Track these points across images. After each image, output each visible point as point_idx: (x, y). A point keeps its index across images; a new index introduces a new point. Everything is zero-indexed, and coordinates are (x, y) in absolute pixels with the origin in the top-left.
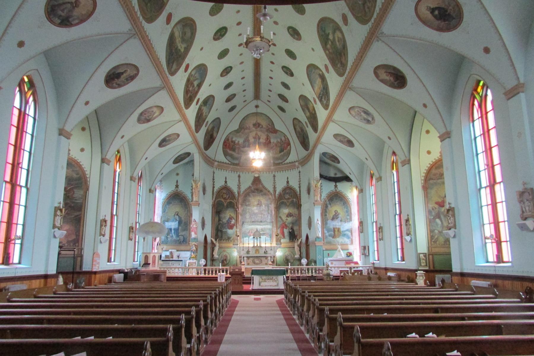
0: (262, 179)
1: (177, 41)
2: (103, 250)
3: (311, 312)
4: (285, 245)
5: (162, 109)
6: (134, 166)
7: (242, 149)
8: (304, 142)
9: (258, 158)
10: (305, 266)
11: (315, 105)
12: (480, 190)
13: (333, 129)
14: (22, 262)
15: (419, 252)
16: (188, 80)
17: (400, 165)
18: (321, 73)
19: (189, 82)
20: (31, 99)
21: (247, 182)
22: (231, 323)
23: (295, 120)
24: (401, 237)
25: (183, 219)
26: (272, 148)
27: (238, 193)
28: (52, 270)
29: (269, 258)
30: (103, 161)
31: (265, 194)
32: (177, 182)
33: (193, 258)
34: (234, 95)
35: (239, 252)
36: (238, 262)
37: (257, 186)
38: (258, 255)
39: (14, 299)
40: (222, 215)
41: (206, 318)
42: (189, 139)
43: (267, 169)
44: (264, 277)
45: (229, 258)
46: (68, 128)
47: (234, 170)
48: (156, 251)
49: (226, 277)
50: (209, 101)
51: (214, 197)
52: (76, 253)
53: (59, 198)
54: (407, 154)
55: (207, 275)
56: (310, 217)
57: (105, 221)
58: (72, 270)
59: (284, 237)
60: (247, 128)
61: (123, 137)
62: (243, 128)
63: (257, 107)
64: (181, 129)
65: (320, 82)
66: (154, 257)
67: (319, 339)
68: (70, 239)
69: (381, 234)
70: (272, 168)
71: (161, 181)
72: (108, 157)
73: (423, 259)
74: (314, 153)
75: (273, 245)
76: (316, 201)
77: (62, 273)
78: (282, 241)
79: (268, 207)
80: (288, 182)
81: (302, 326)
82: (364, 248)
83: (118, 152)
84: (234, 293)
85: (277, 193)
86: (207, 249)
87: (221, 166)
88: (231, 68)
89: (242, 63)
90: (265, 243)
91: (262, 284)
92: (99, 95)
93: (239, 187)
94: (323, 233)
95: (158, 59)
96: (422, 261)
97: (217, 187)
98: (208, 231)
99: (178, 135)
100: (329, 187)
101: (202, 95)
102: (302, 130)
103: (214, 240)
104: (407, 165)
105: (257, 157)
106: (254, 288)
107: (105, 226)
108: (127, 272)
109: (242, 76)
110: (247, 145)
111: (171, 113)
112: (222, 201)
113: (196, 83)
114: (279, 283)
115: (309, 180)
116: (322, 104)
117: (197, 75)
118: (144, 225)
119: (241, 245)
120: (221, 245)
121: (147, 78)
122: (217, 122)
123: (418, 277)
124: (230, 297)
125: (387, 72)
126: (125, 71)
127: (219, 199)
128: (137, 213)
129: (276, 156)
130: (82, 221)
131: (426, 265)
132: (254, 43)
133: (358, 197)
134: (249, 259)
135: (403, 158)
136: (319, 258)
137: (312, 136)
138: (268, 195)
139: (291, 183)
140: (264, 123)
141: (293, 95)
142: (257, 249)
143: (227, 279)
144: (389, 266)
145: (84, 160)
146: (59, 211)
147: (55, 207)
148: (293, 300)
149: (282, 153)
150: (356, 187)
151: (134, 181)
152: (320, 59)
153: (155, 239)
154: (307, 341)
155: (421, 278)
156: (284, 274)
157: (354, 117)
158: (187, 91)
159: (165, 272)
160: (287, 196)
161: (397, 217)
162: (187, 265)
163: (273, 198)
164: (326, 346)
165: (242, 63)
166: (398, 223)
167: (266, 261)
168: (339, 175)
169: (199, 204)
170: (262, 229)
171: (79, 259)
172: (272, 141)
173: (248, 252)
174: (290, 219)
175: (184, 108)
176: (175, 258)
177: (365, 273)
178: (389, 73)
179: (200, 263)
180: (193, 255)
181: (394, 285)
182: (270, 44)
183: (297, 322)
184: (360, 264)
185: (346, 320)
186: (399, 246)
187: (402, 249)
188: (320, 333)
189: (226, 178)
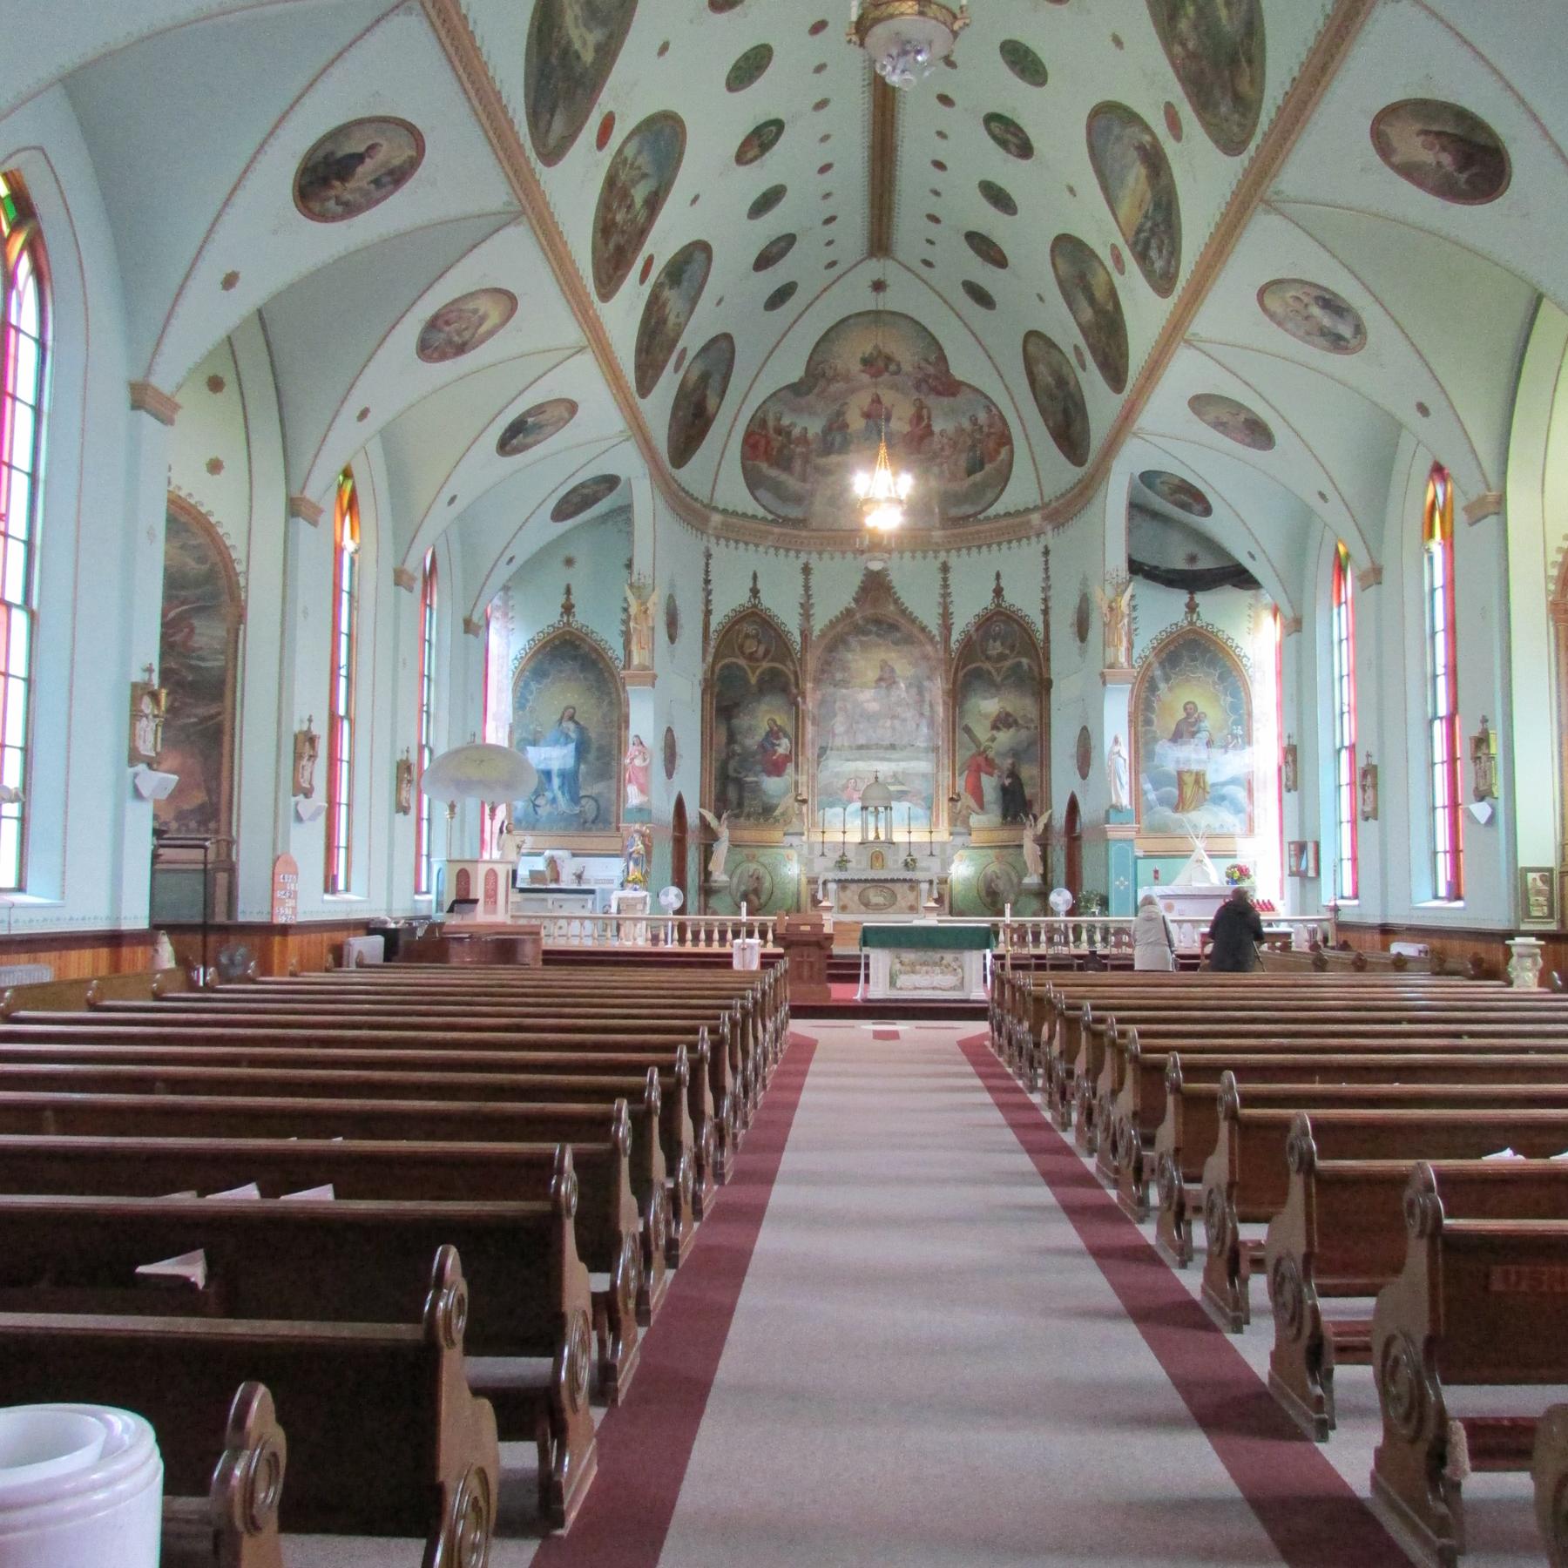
0: (895, 578)
1: (569, 18)
2: (306, 844)
3: (1105, 1083)
4: (985, 836)
5: (509, 301)
6: (405, 531)
7: (822, 461)
8: (1068, 430)
9: (883, 494)
10: (1063, 918)
11: (1117, 280)
12: (1339, 751)
13: (1187, 373)
14: (31, 883)
15: (1522, 863)
16: (611, 182)
17: (1460, 517)
18: (1147, 138)
19: (615, 191)
20: (25, 266)
21: (836, 593)
22: (799, 1117)
23: (1036, 344)
24: (1454, 805)
25: (593, 735)
26: (935, 456)
27: (805, 635)
28: (136, 917)
29: (925, 886)
30: (295, 507)
31: (908, 640)
32: (568, 591)
33: (634, 882)
34: (789, 240)
35: (807, 863)
36: (805, 899)
37: (876, 611)
38: (881, 875)
39: (23, 1014)
40: (742, 721)
41: (719, 1090)
42: (616, 422)
43: (914, 542)
44: (909, 956)
45: (767, 884)
46: (164, 380)
47: (785, 546)
48: (496, 855)
49: (763, 956)
50: (690, 265)
51: (712, 650)
52: (211, 856)
53: (147, 652)
54: (1493, 479)
55: (689, 948)
56: (1084, 729)
57: (312, 740)
58: (204, 921)
59: (981, 805)
60: (834, 379)
61: (364, 414)
62: (824, 375)
63: (879, 286)
64: (582, 379)
65: (1143, 179)
66: (492, 875)
67: (1138, 1170)
68: (186, 807)
69: (1370, 792)
70: (938, 534)
71: (506, 588)
72: (311, 494)
73: (1539, 892)
74: (1108, 471)
75: (936, 837)
76: (1111, 666)
77: (174, 929)
78: (975, 820)
79: (920, 692)
80: (998, 592)
81: (1065, 1130)
82: (1301, 848)
83: (347, 474)
84: (799, 1012)
85: (955, 636)
86: (685, 848)
87: (737, 529)
88: (778, 125)
89: (821, 105)
90: (908, 829)
91: (903, 980)
92: (275, 246)
93: (806, 614)
94: (1137, 793)
95: (498, 95)
96: (1532, 899)
97: (722, 612)
98: (690, 781)
99: (572, 407)
100: (1164, 610)
101: (663, 242)
102: (1061, 382)
103: (710, 817)
104: (1492, 519)
105: (880, 493)
106: (871, 996)
107: (313, 757)
108: (396, 931)
109: (822, 158)
110: (836, 439)
111: (546, 320)
112: (739, 667)
113: (639, 194)
114: (971, 977)
115: (1084, 581)
116: (1149, 274)
117: (644, 161)
118: (453, 755)
119: (817, 838)
120: (738, 833)
121: (458, 174)
122: (721, 350)
123: (1514, 960)
124: (784, 1025)
125: (1426, 133)
126: (372, 148)
127: (726, 661)
128: (423, 710)
129: (955, 487)
130: (226, 738)
131: (1551, 915)
132: (894, 25)
133: (1280, 649)
134: (844, 888)
135: (1476, 490)
136: (1117, 885)
137: (1101, 404)
138: (921, 644)
139: (1012, 598)
140: (906, 355)
141: (1029, 240)
142: (877, 851)
143: (767, 961)
144: (1396, 917)
145: (221, 503)
146: (147, 700)
147: (135, 686)
148: (1029, 1038)
149: (978, 477)
150: (1276, 611)
151: (410, 590)
152: (1148, 80)
153: (493, 810)
154: (1086, 1180)
155: (1528, 962)
156: (988, 946)
157: (1280, 324)
158: (605, 228)
159: (535, 933)
160: (995, 648)
161: (1439, 729)
162: (614, 909)
163: (941, 653)
164: (1167, 1195)
165: (821, 105)
166: (1440, 753)
167: (911, 896)
168: (1205, 563)
169: (655, 677)
170: (895, 775)
171: (222, 878)
172: (936, 428)
173: (842, 863)
174: (1004, 737)
175: (594, 297)
176: (567, 882)
177: (1300, 943)
178: (1439, 134)
179: (663, 900)
180: (635, 873)
181: (1418, 988)
182: (956, 27)
183: (1048, 1115)
184: (1283, 909)
185: (1250, 1100)
186: (1443, 842)
187: (1455, 852)
188: (1147, 1153)
189: (755, 577)
